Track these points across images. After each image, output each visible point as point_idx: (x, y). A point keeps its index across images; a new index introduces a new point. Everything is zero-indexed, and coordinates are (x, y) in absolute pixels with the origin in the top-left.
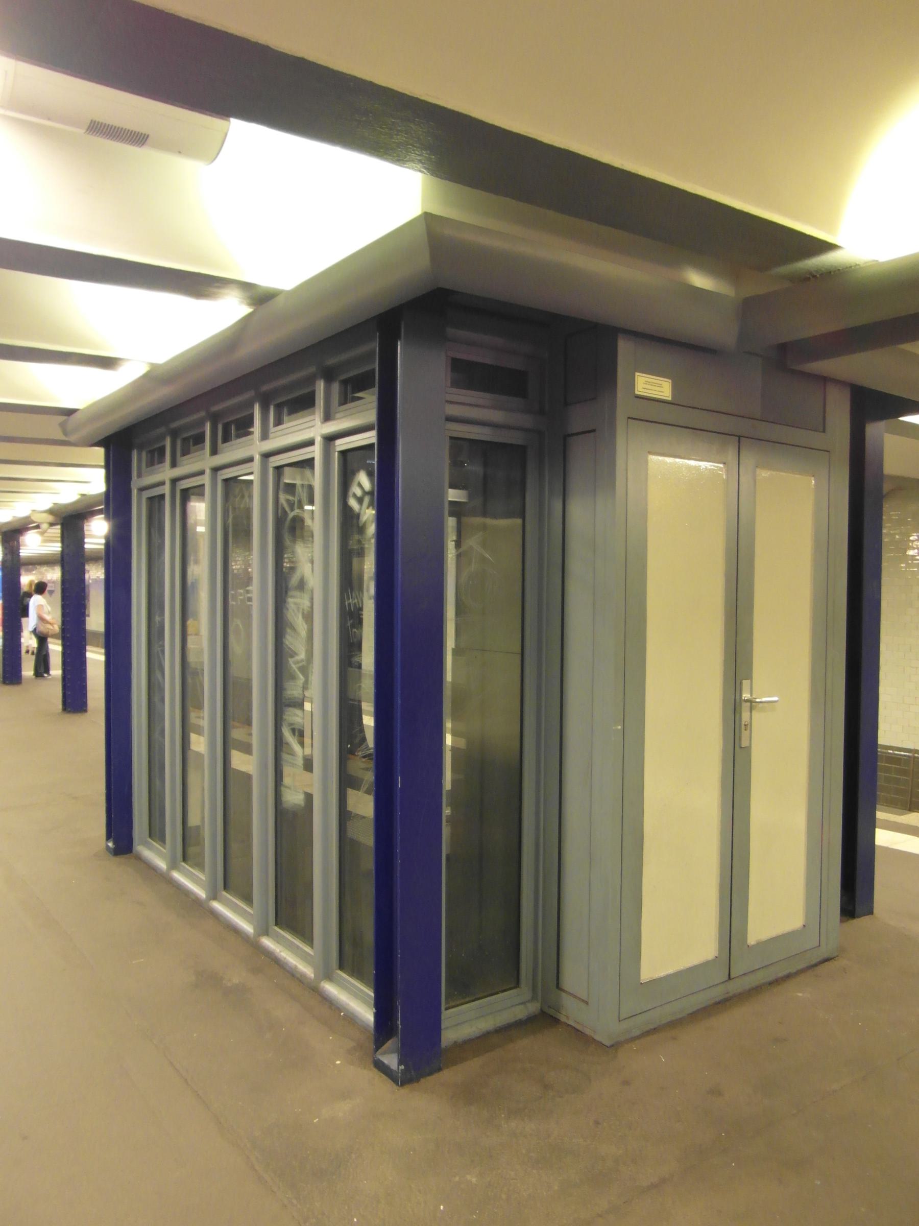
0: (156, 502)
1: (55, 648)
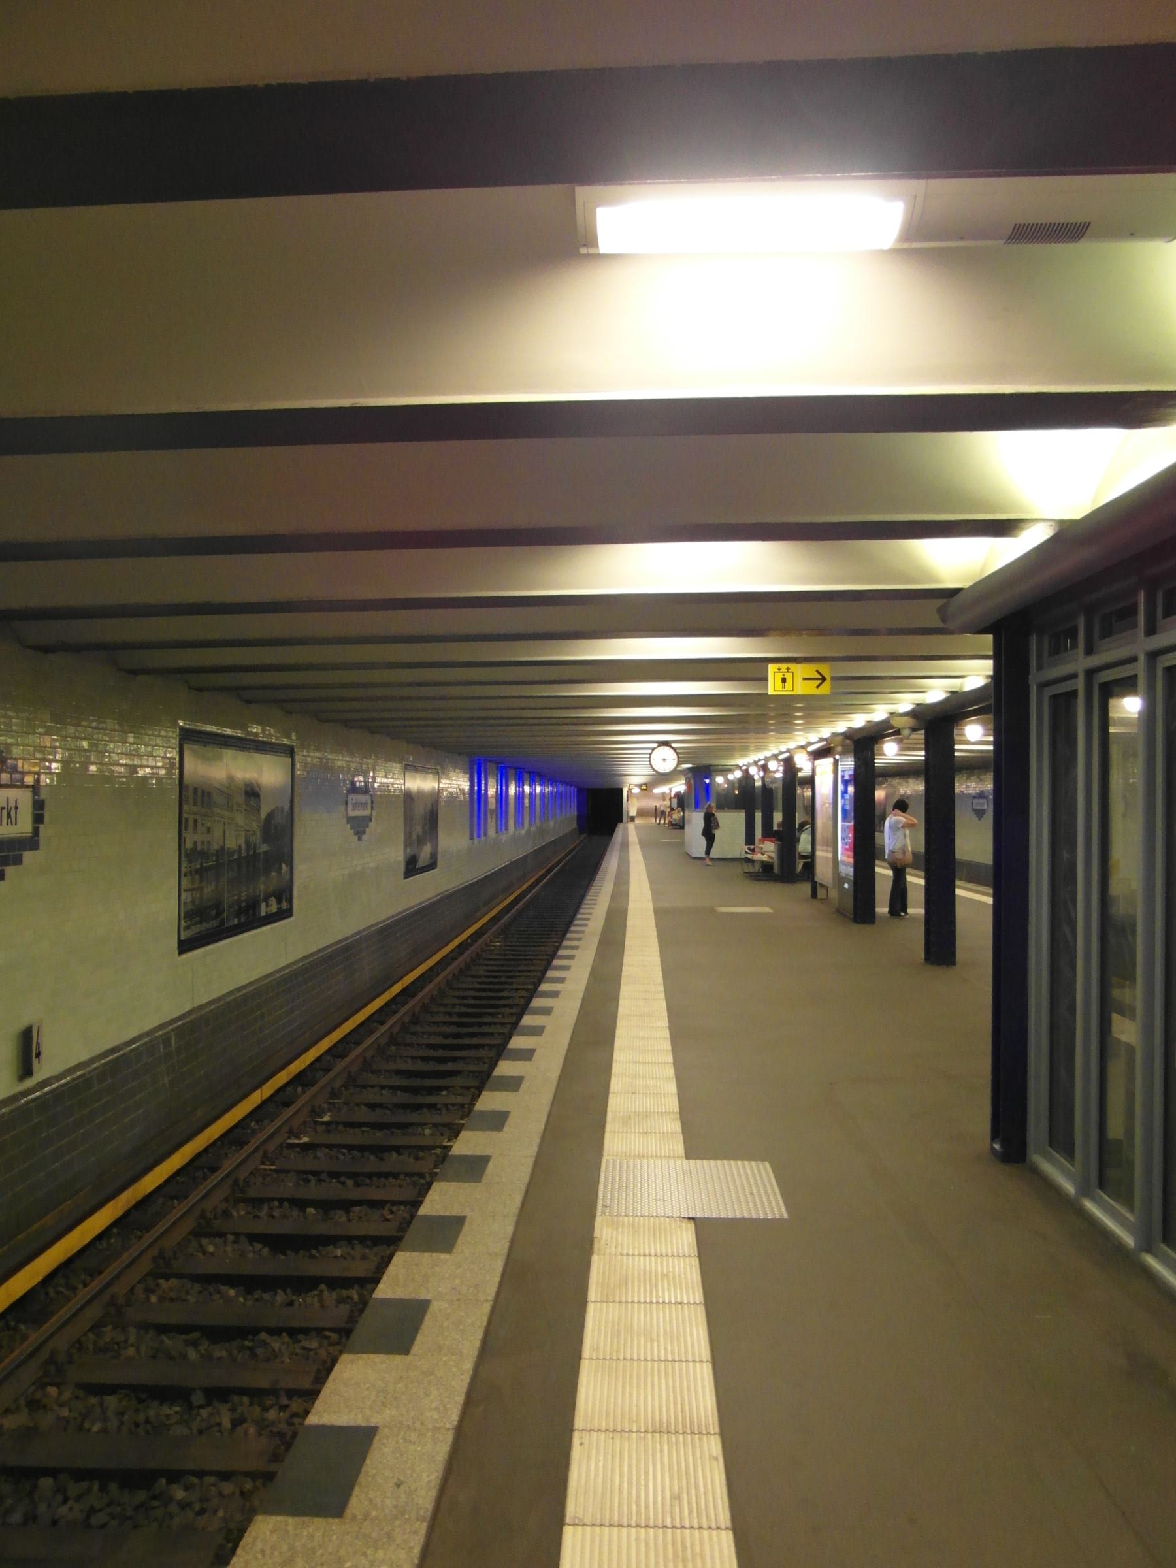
0: (1063, 705)
1: (916, 881)
